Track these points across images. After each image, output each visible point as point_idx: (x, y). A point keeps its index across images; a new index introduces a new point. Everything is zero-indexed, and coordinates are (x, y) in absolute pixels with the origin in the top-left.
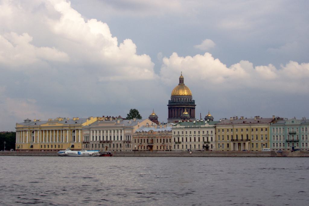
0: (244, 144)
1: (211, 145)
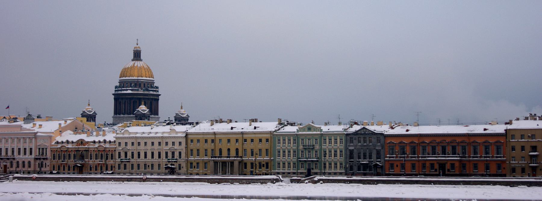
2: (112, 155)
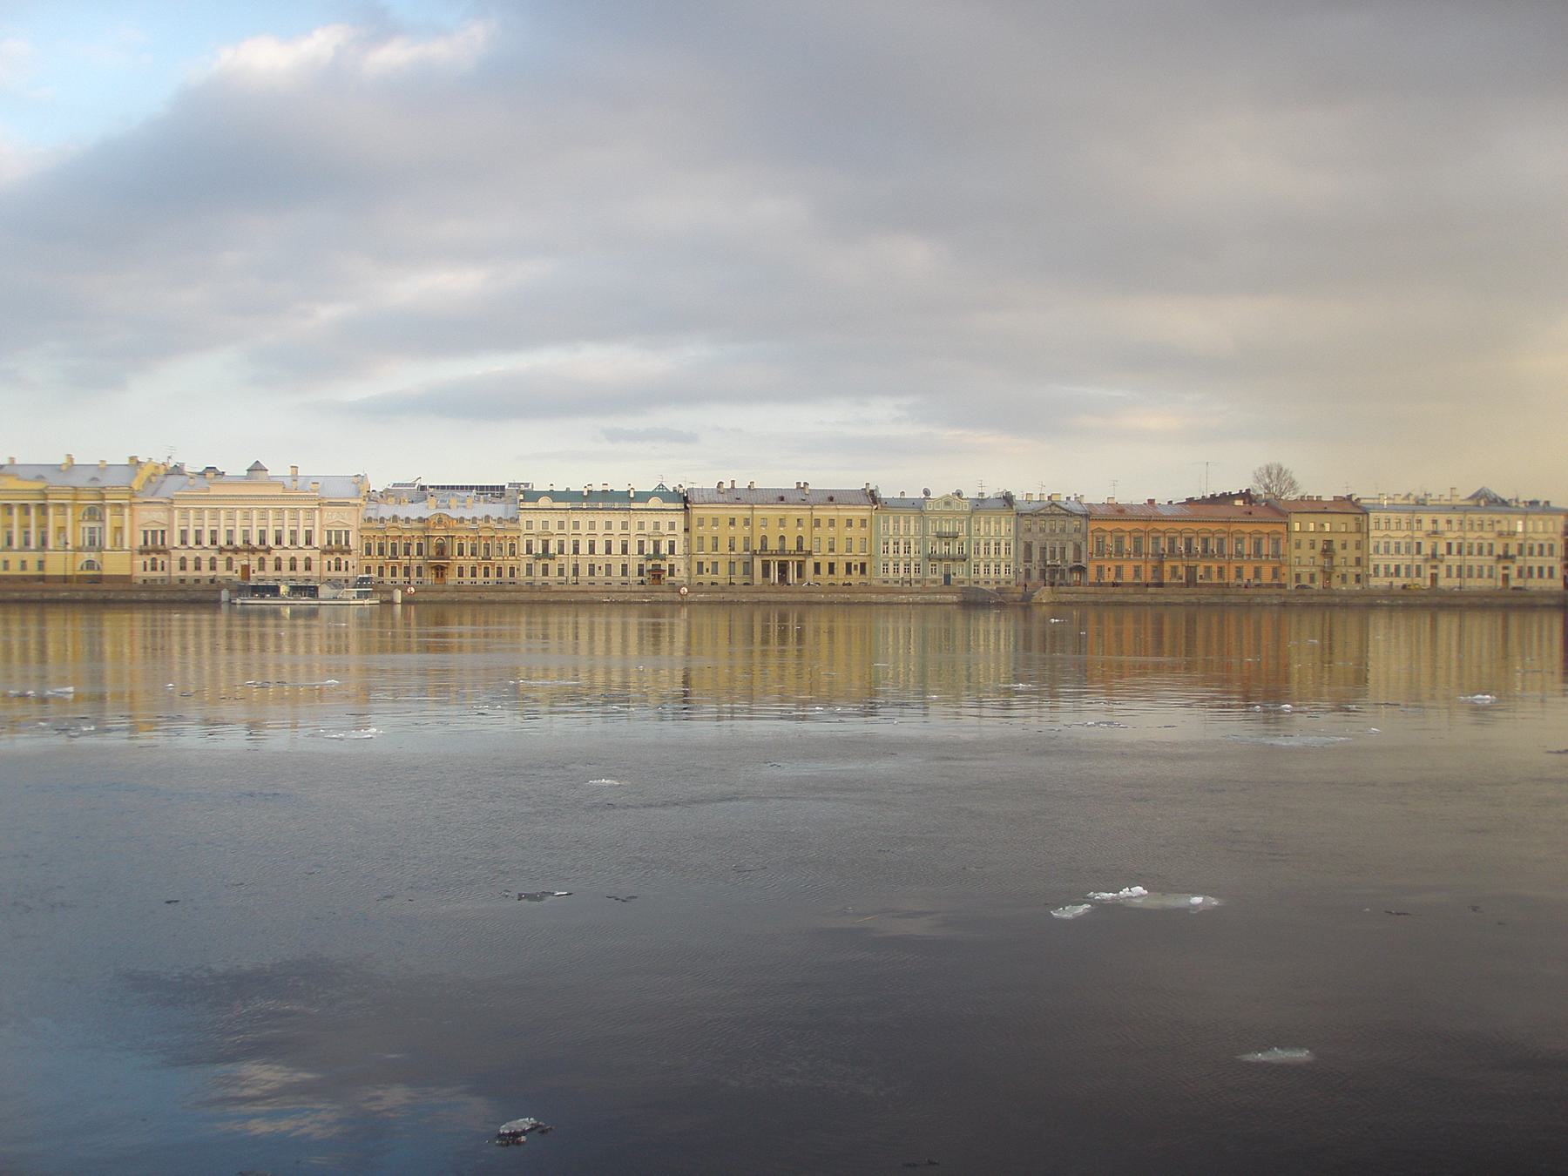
2: (512, 545)
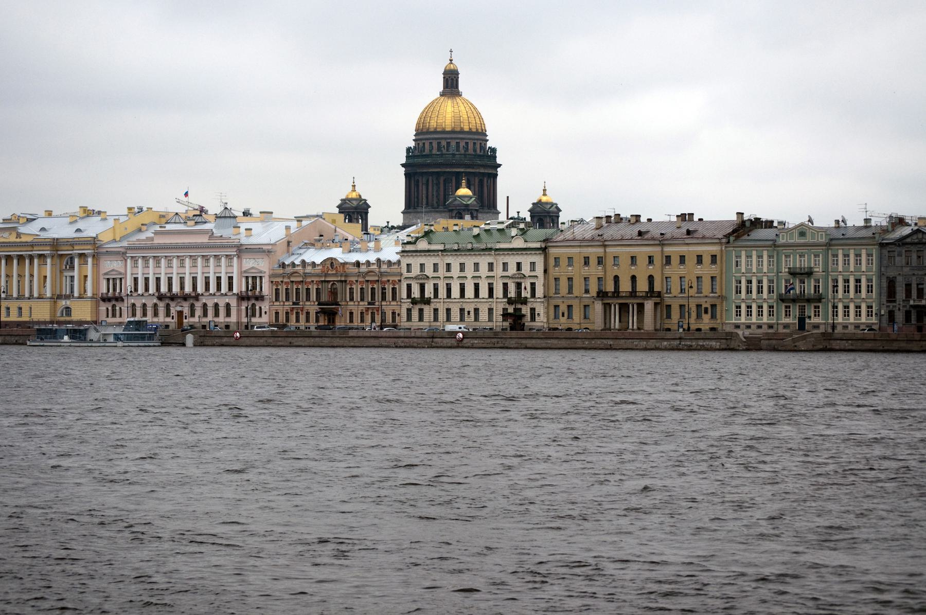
0: (641, 307)
1: (529, 310)
2: (394, 289)
